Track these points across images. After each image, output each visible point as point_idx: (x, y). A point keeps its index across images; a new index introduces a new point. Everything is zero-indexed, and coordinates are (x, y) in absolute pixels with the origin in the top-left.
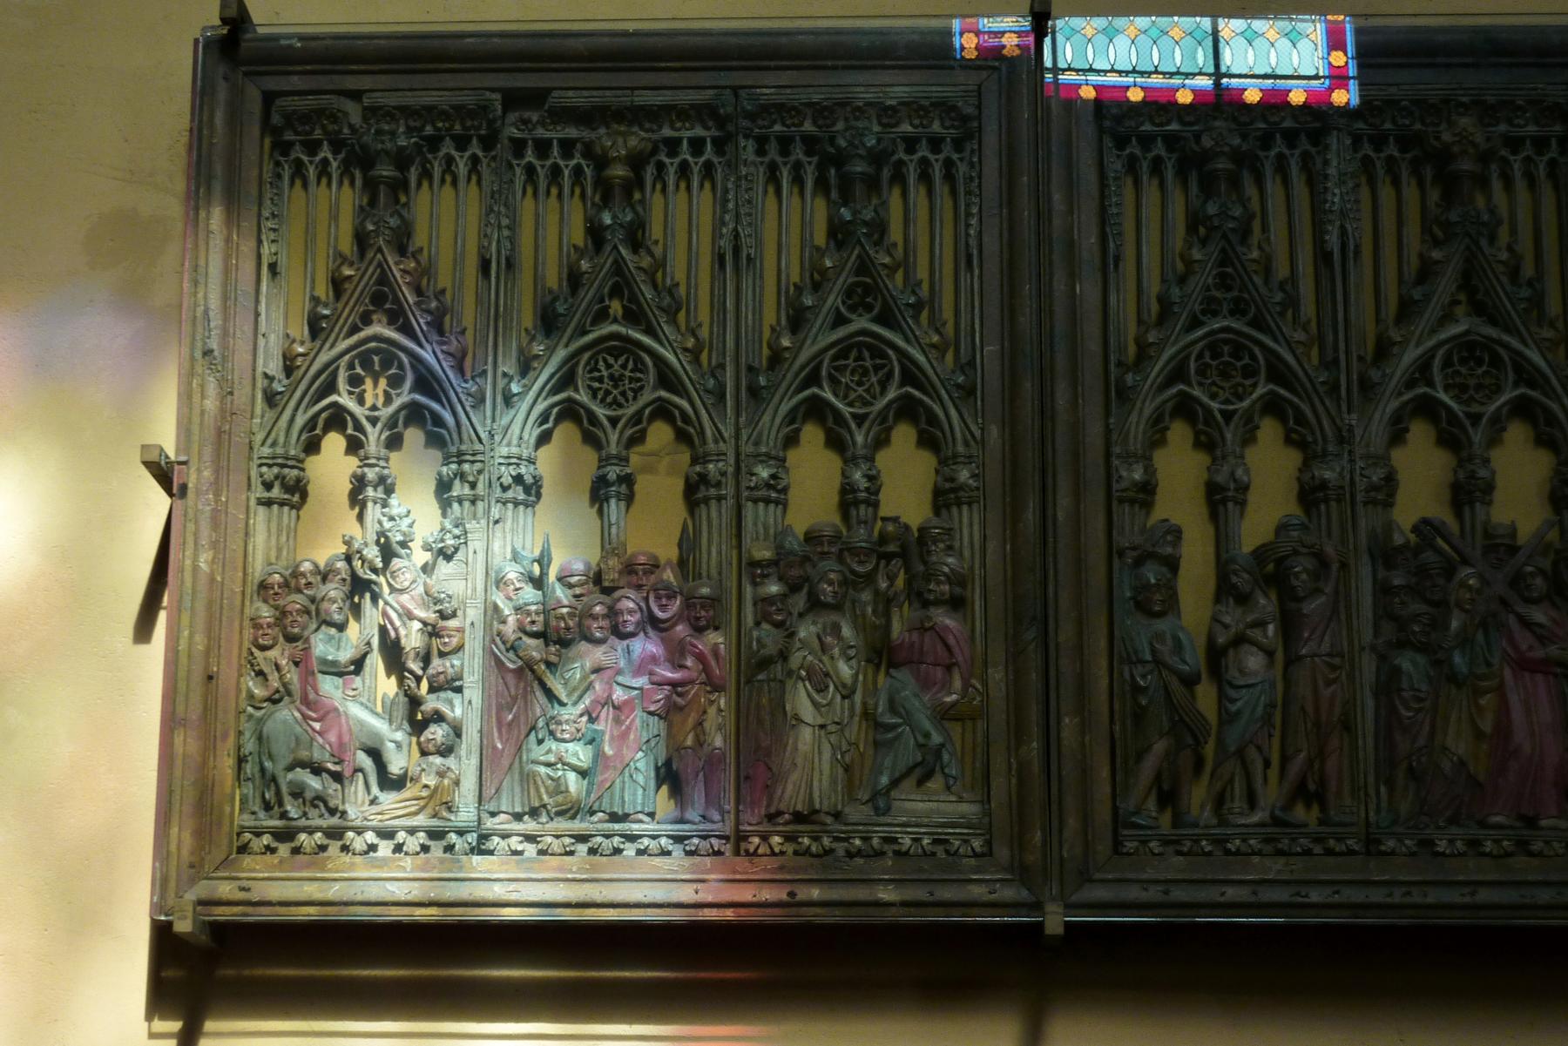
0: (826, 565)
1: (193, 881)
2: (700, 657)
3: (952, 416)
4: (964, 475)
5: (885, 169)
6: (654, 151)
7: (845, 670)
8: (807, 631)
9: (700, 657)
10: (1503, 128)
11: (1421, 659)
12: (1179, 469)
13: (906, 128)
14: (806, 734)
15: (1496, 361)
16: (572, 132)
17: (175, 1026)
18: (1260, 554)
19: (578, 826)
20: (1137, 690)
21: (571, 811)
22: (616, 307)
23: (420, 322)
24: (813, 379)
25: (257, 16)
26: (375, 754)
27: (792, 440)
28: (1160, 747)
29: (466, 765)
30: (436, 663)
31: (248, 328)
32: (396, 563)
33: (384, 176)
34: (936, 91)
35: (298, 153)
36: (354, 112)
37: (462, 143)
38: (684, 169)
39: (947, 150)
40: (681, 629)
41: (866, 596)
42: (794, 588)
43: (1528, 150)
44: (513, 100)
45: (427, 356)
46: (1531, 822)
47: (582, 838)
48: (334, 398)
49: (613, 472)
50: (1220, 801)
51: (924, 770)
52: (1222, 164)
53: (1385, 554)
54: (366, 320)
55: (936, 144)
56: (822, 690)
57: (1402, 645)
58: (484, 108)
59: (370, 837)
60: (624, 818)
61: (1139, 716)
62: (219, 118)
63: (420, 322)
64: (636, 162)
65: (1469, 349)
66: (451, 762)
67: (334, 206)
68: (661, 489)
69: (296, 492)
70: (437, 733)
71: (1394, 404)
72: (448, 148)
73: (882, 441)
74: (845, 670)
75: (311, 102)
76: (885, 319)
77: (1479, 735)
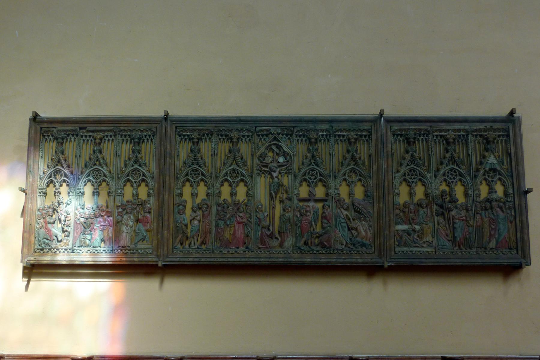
0: (129, 206)
1: (27, 257)
2: (108, 221)
3: (149, 181)
4: (151, 192)
5: (140, 141)
6: (104, 137)
7: (131, 223)
8: (125, 217)
9: (108, 221)
10: (242, 133)
11: (222, 222)
12: (187, 190)
13: (145, 133)
14: (125, 234)
15: (238, 173)
16: (91, 134)
17: (27, 279)
18: (198, 205)
19: (88, 248)
20: (177, 227)
21: (88, 246)
22: (97, 163)
23: (65, 166)
24: (128, 175)
25: (170, 114)
26: (56, 237)
27: (125, 185)
28: (180, 236)
29: (71, 239)
30: (67, 222)
31: (37, 167)
32: (60, 206)
33: (61, 141)
34: (150, 128)
35: (46, 137)
36: (55, 130)
37: (73, 135)
38: (325, 140)
39: (152, 137)
40: (106, 217)
41: (135, 211)
42: (124, 210)
43: (246, 137)
44: (81, 128)
45: (66, 171)
46: (238, 248)
47: (89, 250)
48: (226, 177)
49: (96, 191)
50: (190, 244)
51: (143, 240)
52: (196, 140)
53: (218, 205)
54: (57, 165)
55: (150, 136)
56: (127, 227)
57: (220, 219)
58: (76, 130)
59: (55, 250)
60: (95, 247)
61: (177, 231)
62: (33, 132)
63: (65, 166)
64: (101, 139)
65: (234, 171)
66: (68, 238)
67: (52, 145)
68: (104, 193)
69: (45, 194)
70: (66, 233)
71: (221, 180)
72: (71, 136)
73: (139, 186)
74: (131, 223)
75: (48, 129)
76: (140, 166)
77: (230, 234)
